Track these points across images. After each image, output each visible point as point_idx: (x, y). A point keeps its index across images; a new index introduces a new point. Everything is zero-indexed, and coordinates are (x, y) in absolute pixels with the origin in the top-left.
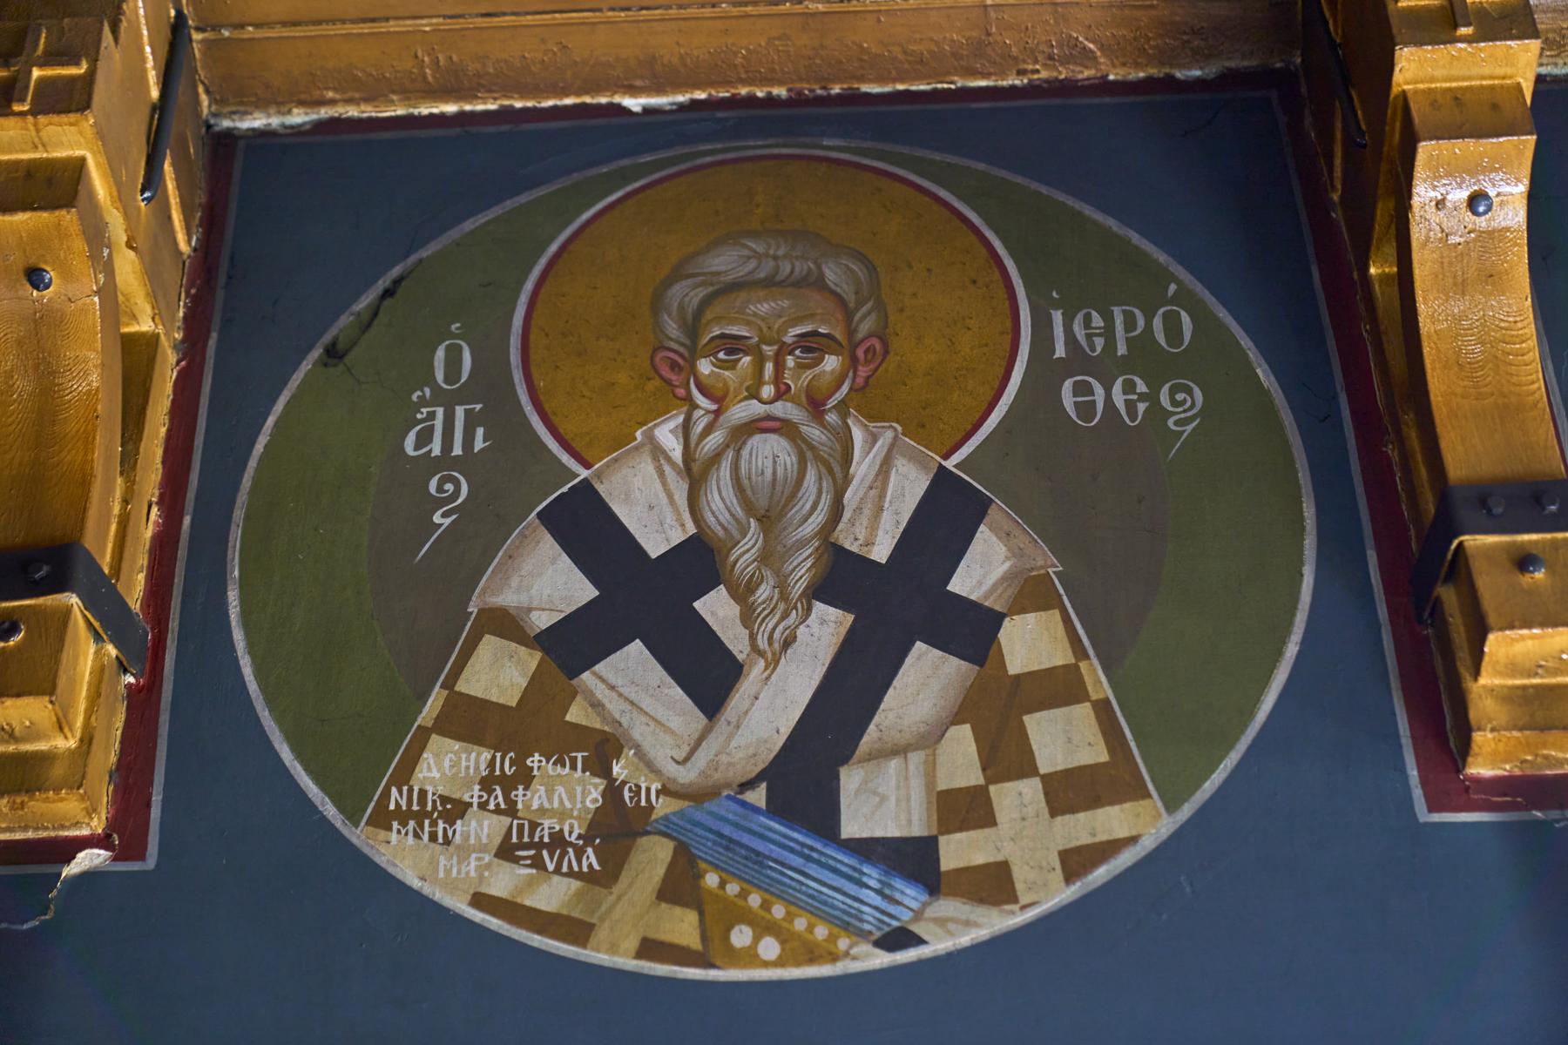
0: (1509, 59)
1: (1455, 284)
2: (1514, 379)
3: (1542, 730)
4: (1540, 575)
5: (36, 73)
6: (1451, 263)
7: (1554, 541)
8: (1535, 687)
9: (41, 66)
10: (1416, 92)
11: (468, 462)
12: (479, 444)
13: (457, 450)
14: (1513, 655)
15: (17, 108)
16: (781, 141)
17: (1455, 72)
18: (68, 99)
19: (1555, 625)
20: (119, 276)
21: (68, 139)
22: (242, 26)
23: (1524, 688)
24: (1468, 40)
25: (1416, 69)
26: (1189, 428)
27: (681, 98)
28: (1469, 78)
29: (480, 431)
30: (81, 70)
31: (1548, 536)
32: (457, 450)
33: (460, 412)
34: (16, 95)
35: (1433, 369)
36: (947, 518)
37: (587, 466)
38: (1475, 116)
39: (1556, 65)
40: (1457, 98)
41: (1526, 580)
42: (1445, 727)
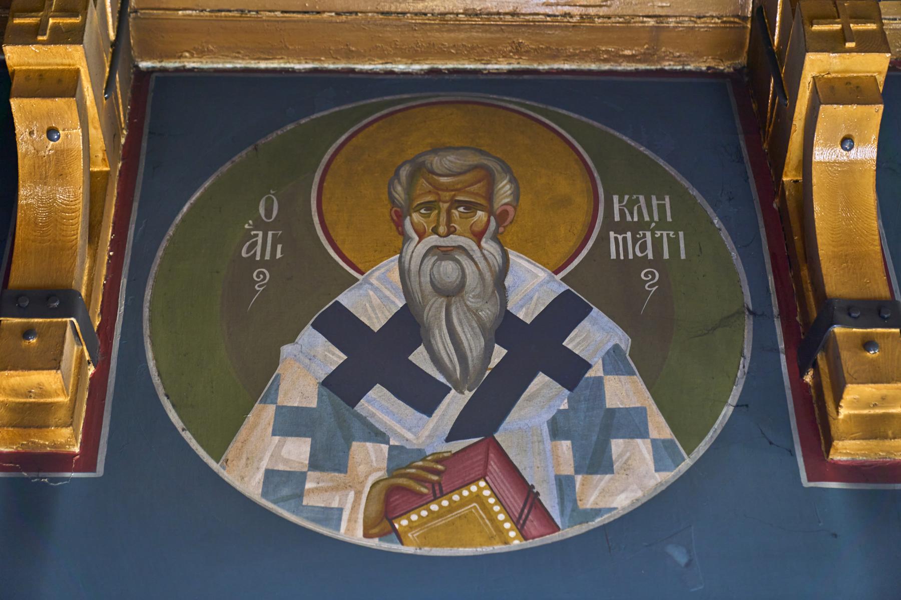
0: (69, 55)
1: (41, 179)
2: (64, 233)
3: (25, 427)
4: (33, 341)
5: (51, 21)
6: (39, 167)
7: (51, 323)
8: (31, 403)
9: (53, 17)
10: (20, 70)
11: (270, 265)
12: (279, 255)
13: (267, 257)
14: (855, 400)
15: (40, 38)
16: (418, 95)
17: (40, 61)
18: (73, 36)
19: (30, 369)
20: (67, 143)
21: (74, 57)
22: (356, 13)
23: (25, 403)
24: (43, 43)
25: (817, 64)
26: (654, 289)
27: (426, 67)
28: (49, 64)
29: (279, 247)
30: (77, 20)
31: (49, 320)
32: (267, 257)
33: (270, 234)
34: (40, 32)
35: (21, 225)
36: (565, 313)
37: (362, 273)
38: (847, 91)
39: (201, 62)
40: (41, 74)
41: (25, 343)
42: (818, 431)
